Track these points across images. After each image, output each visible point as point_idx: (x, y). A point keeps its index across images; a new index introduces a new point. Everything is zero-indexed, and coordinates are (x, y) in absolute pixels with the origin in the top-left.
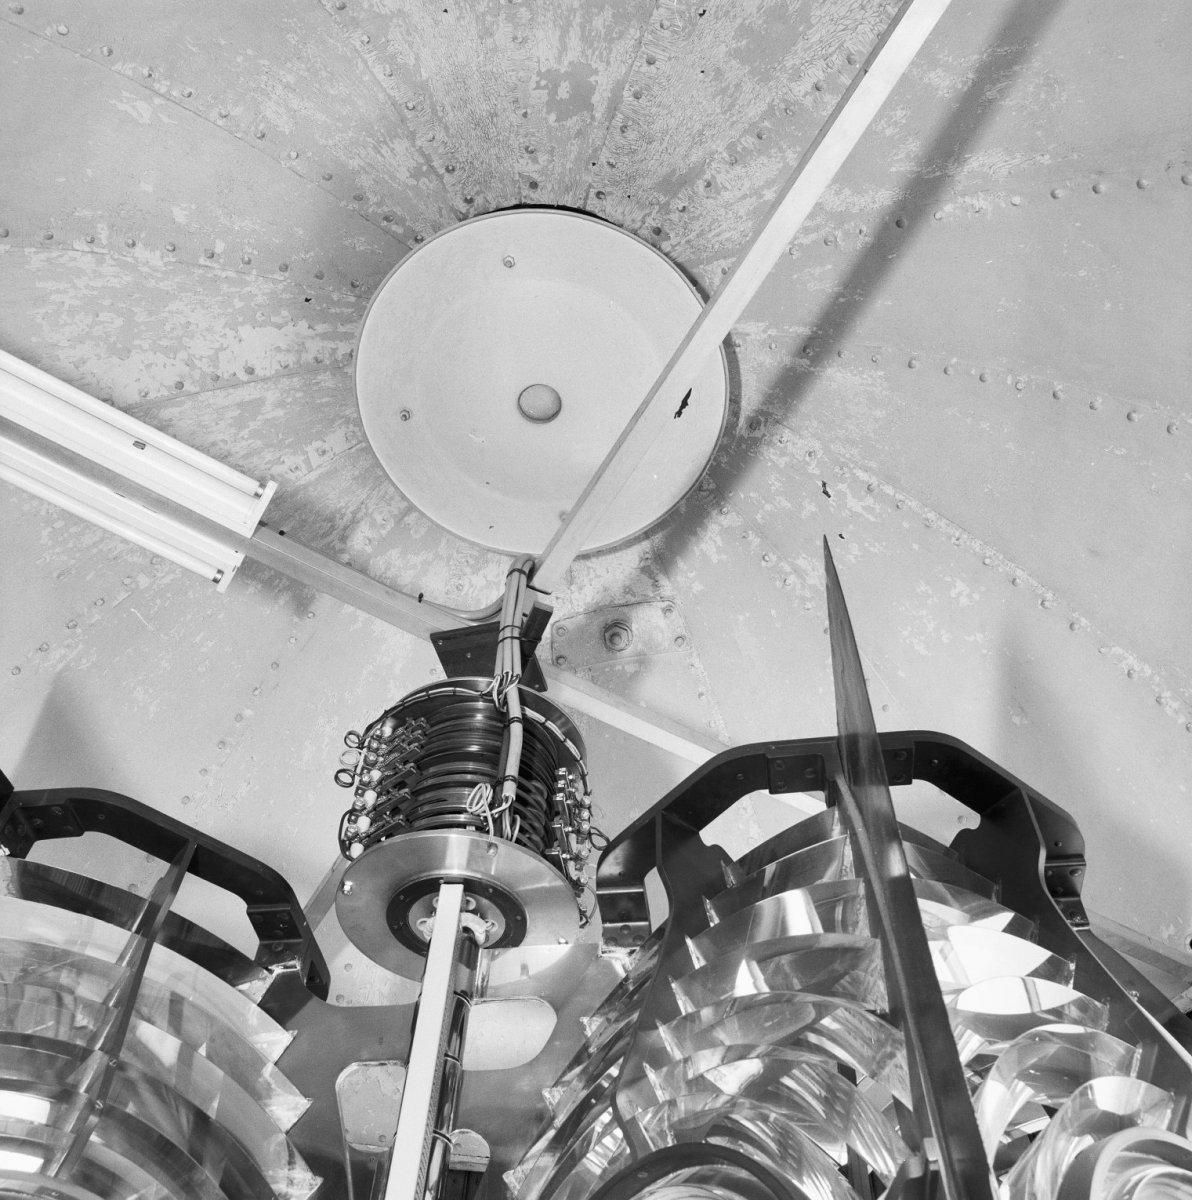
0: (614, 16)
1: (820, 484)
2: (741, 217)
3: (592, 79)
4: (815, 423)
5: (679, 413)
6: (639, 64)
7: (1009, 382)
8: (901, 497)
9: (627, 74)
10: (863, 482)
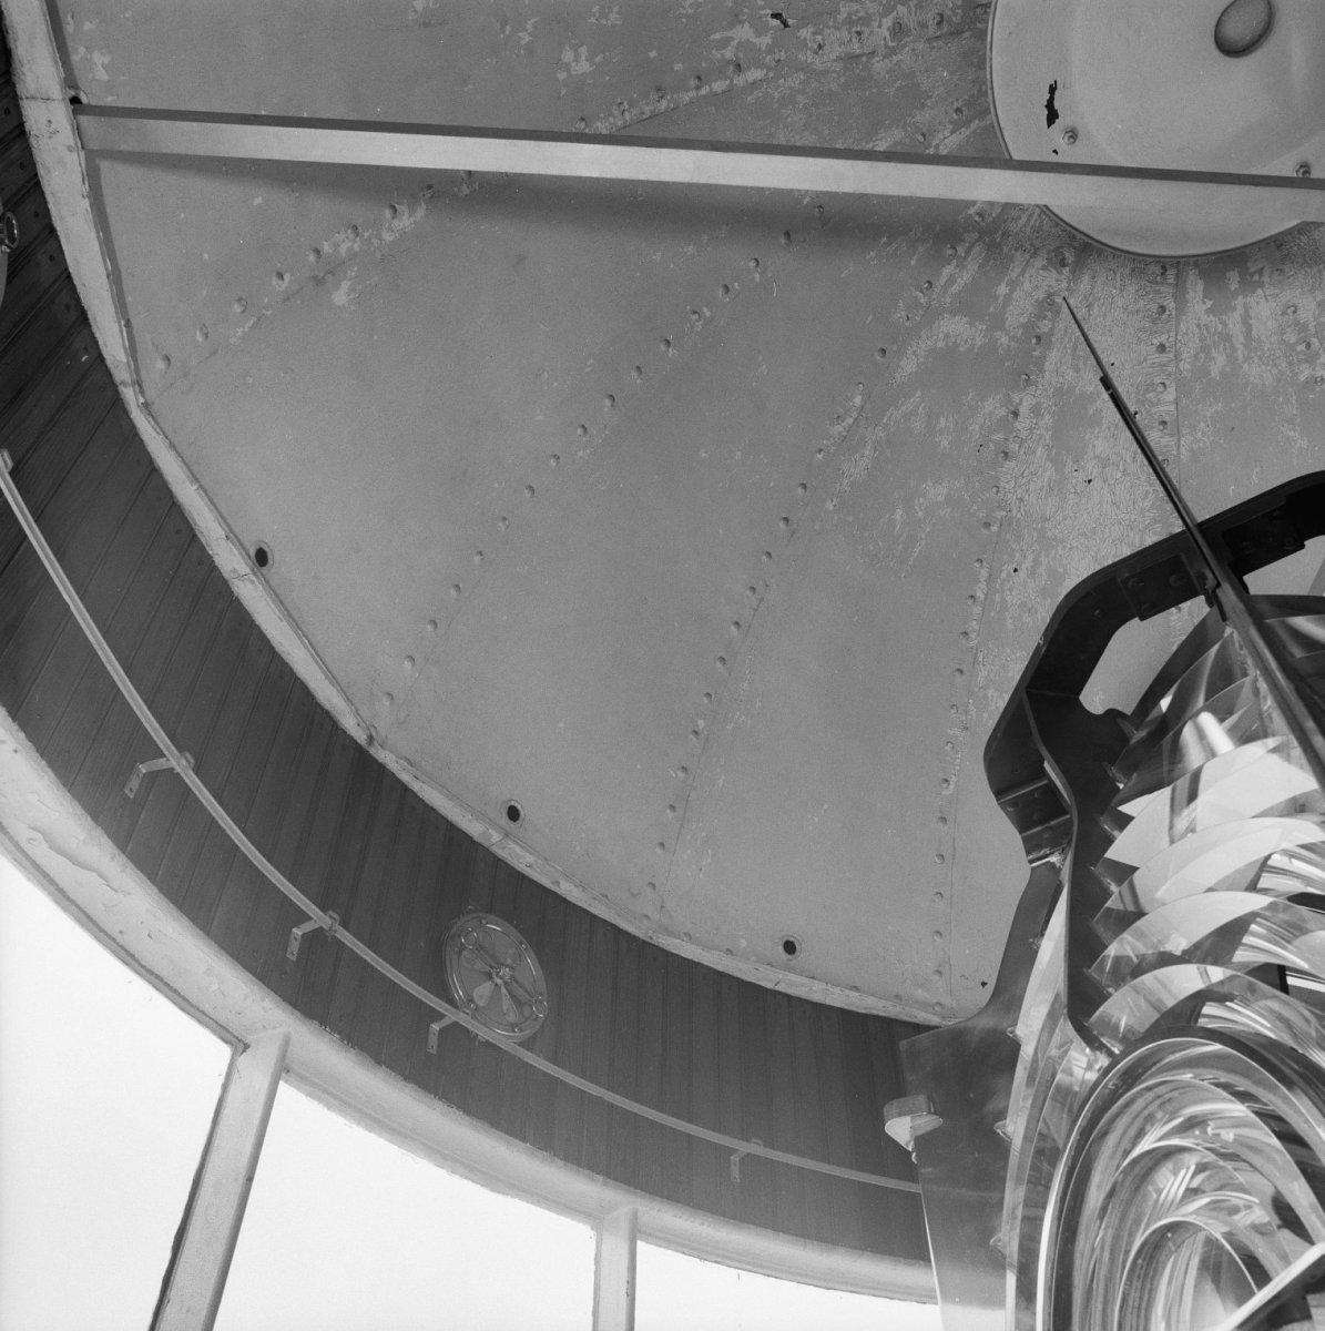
0: (1209, 372)
1: (790, 22)
2: (1016, 250)
3: (1209, 304)
4: (834, 86)
5: (1052, 89)
6: (1171, 339)
7: (705, 310)
8: (703, 92)
9: (1178, 324)
10: (749, 68)
